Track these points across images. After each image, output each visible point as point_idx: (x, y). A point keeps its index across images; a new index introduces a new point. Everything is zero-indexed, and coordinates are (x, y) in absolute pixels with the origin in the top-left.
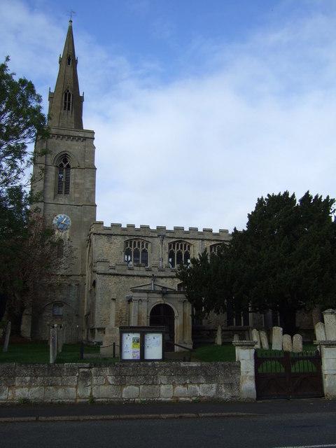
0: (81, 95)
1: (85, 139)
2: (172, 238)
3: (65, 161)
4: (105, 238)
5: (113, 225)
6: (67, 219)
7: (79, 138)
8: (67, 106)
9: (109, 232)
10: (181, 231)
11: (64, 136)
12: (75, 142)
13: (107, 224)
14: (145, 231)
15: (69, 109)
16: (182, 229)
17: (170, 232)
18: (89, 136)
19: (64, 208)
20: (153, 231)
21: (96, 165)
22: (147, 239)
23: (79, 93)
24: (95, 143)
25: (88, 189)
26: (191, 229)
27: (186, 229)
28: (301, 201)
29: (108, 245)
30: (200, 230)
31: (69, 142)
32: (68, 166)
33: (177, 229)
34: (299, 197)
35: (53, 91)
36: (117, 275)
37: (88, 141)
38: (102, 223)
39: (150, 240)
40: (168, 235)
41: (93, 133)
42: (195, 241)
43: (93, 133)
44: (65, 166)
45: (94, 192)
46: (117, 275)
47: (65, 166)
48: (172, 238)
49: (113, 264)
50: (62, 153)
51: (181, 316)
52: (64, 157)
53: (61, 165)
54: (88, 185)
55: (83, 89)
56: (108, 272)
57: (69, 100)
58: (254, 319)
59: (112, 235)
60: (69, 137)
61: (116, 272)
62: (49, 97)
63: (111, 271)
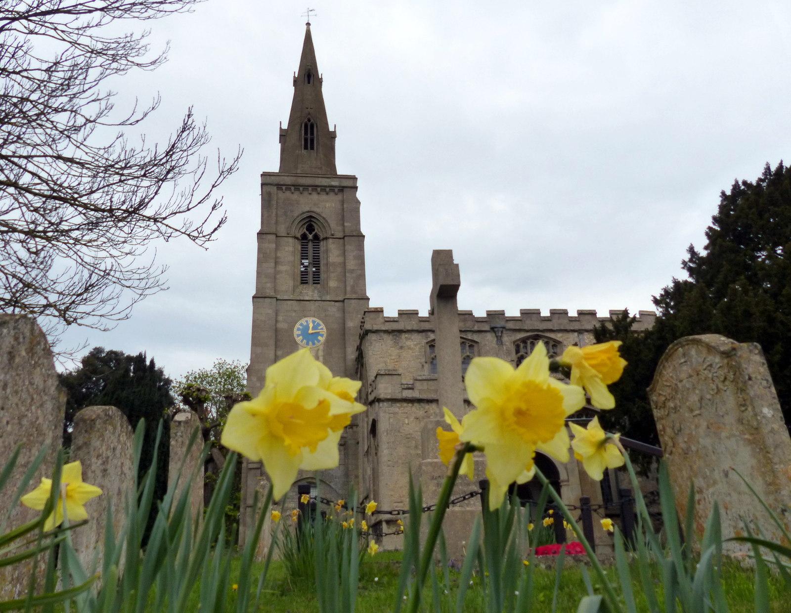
0: (331, 129)
1: (342, 189)
2: (520, 330)
3: (310, 229)
4: (388, 339)
5: (402, 313)
6: (314, 322)
7: (332, 188)
8: (309, 144)
9: (395, 326)
10: (534, 317)
11: (306, 187)
12: (324, 197)
13: (391, 312)
14: (465, 320)
15: (312, 148)
16: (537, 312)
17: (513, 319)
18: (348, 185)
19: (312, 306)
20: (479, 321)
21: (363, 230)
22: (552, 335)
23: (327, 124)
24: (359, 195)
25: (352, 271)
26: (553, 312)
27: (545, 313)
28: (691, 275)
29: (395, 352)
30: (573, 313)
31: (315, 196)
32: (316, 238)
33: (526, 313)
34: (684, 276)
35: (285, 126)
36: (420, 401)
37: (347, 193)
38: (380, 311)
39: (476, 337)
40: (510, 325)
41: (354, 178)
42: (566, 335)
43: (354, 178)
44: (310, 237)
45: (362, 276)
46: (420, 401)
47: (310, 237)
48: (520, 330)
49: (407, 380)
50: (305, 216)
51: (178, 494)
52: (310, 223)
53: (304, 237)
54: (351, 264)
55: (335, 117)
56: (399, 396)
57: (312, 134)
58: (472, 513)
59: (401, 332)
60: (315, 187)
61: (415, 394)
62: (281, 136)
63: (408, 394)
